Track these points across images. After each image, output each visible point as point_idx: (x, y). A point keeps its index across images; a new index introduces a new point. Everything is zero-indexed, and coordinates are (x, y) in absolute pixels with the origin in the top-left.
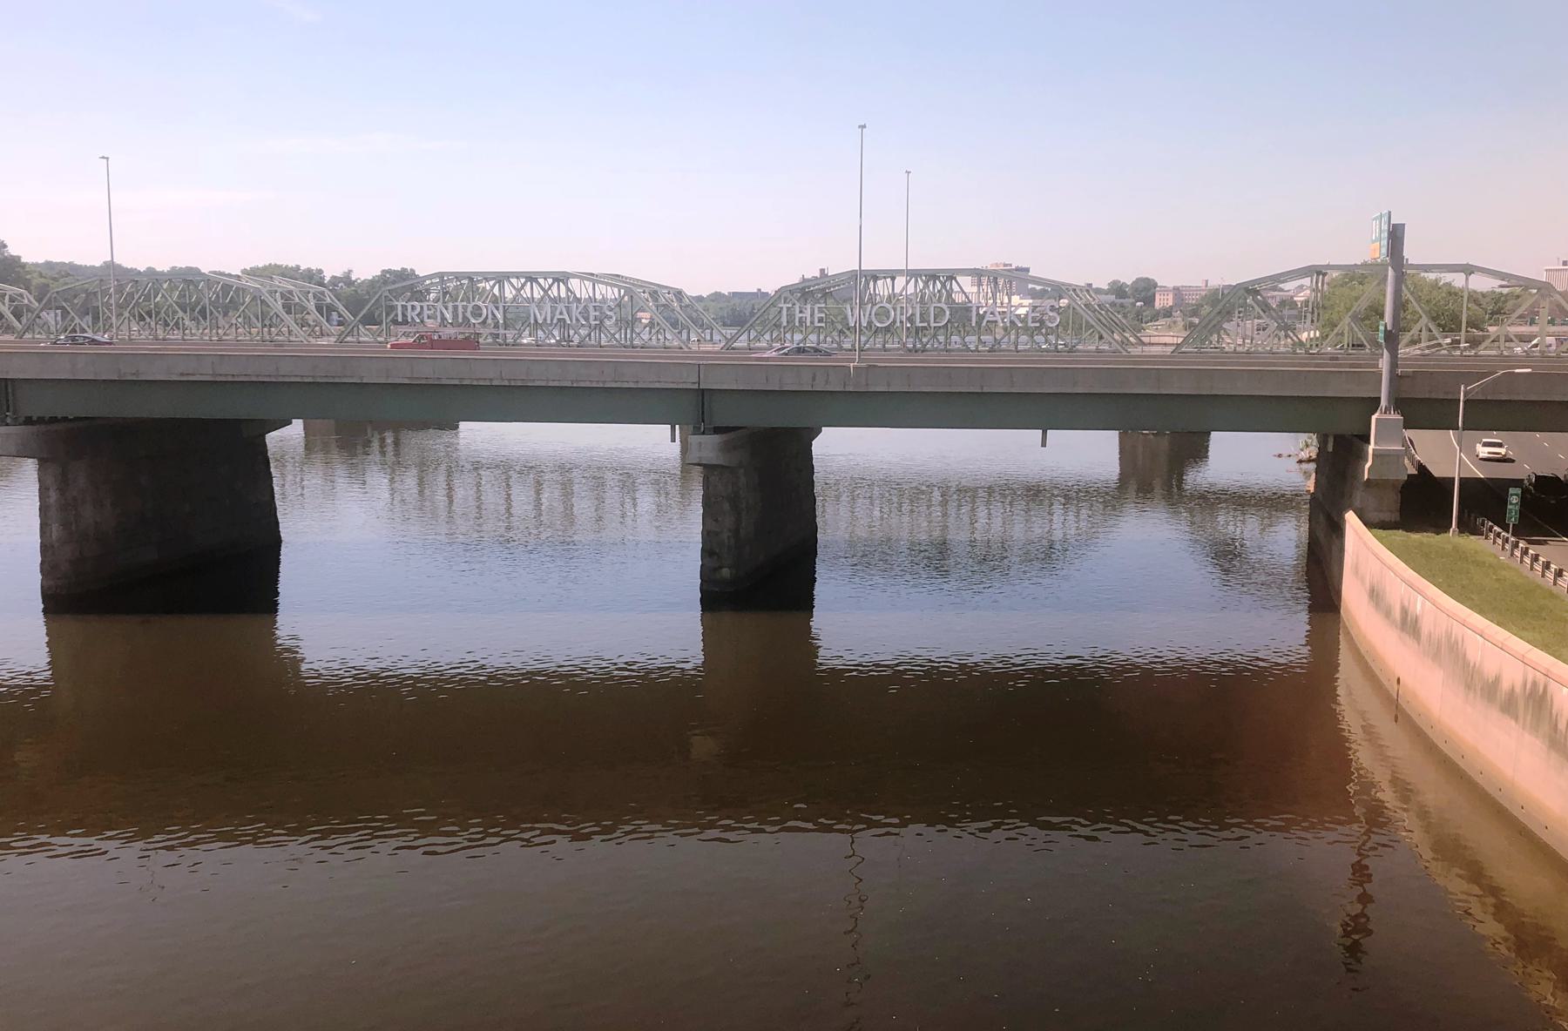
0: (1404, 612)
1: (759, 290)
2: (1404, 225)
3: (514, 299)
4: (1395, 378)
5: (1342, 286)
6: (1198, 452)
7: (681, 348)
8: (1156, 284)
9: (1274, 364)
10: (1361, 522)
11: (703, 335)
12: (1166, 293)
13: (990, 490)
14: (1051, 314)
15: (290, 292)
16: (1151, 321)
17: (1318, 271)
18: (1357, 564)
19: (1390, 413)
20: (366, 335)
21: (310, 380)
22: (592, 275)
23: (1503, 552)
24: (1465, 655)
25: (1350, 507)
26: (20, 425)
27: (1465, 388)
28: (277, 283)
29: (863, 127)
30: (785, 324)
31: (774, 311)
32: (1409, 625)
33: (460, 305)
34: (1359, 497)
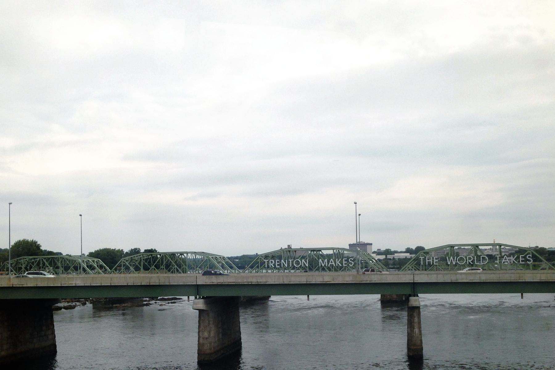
21: (509, 281)
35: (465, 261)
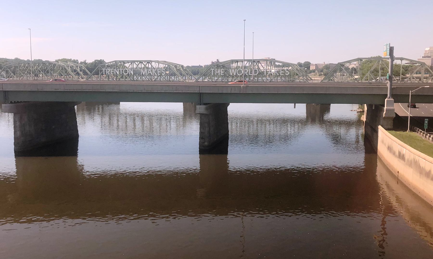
0: (400, 153)
1: (200, 65)
2: (393, 47)
3: (136, 68)
4: (392, 89)
5: (365, 63)
6: (327, 109)
7: (183, 81)
8: (310, 63)
9: (342, 85)
10: (383, 128)
11: (189, 78)
12: (313, 66)
13: (269, 121)
14: (287, 72)
15: (73, 66)
16: (310, 73)
17: (361, 60)
18: (383, 140)
19: (390, 98)
20: (94, 78)
22: (158, 61)
23: (423, 137)
24: (420, 164)
25: (379, 125)
26: (9, 104)
27: (411, 91)
28: (69, 64)
29: (245, 20)
30: (213, 75)
31: (209, 71)
32: (401, 157)
33: (121, 70)
34: (382, 121)
35: (258, 71)
